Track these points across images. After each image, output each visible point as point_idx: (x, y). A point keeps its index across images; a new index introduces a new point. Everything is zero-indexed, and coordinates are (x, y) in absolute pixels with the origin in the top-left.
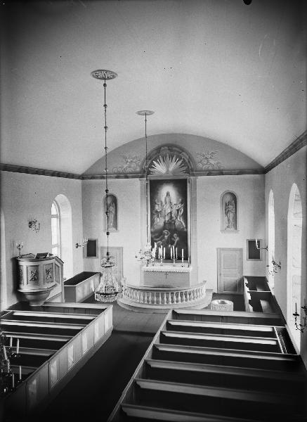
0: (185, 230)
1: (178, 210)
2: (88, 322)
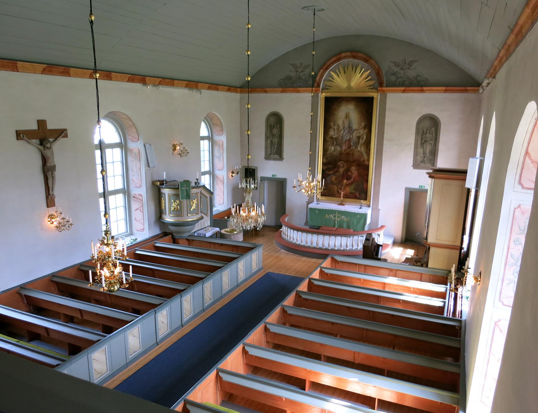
0: (367, 163)
1: (359, 138)
2: (230, 260)
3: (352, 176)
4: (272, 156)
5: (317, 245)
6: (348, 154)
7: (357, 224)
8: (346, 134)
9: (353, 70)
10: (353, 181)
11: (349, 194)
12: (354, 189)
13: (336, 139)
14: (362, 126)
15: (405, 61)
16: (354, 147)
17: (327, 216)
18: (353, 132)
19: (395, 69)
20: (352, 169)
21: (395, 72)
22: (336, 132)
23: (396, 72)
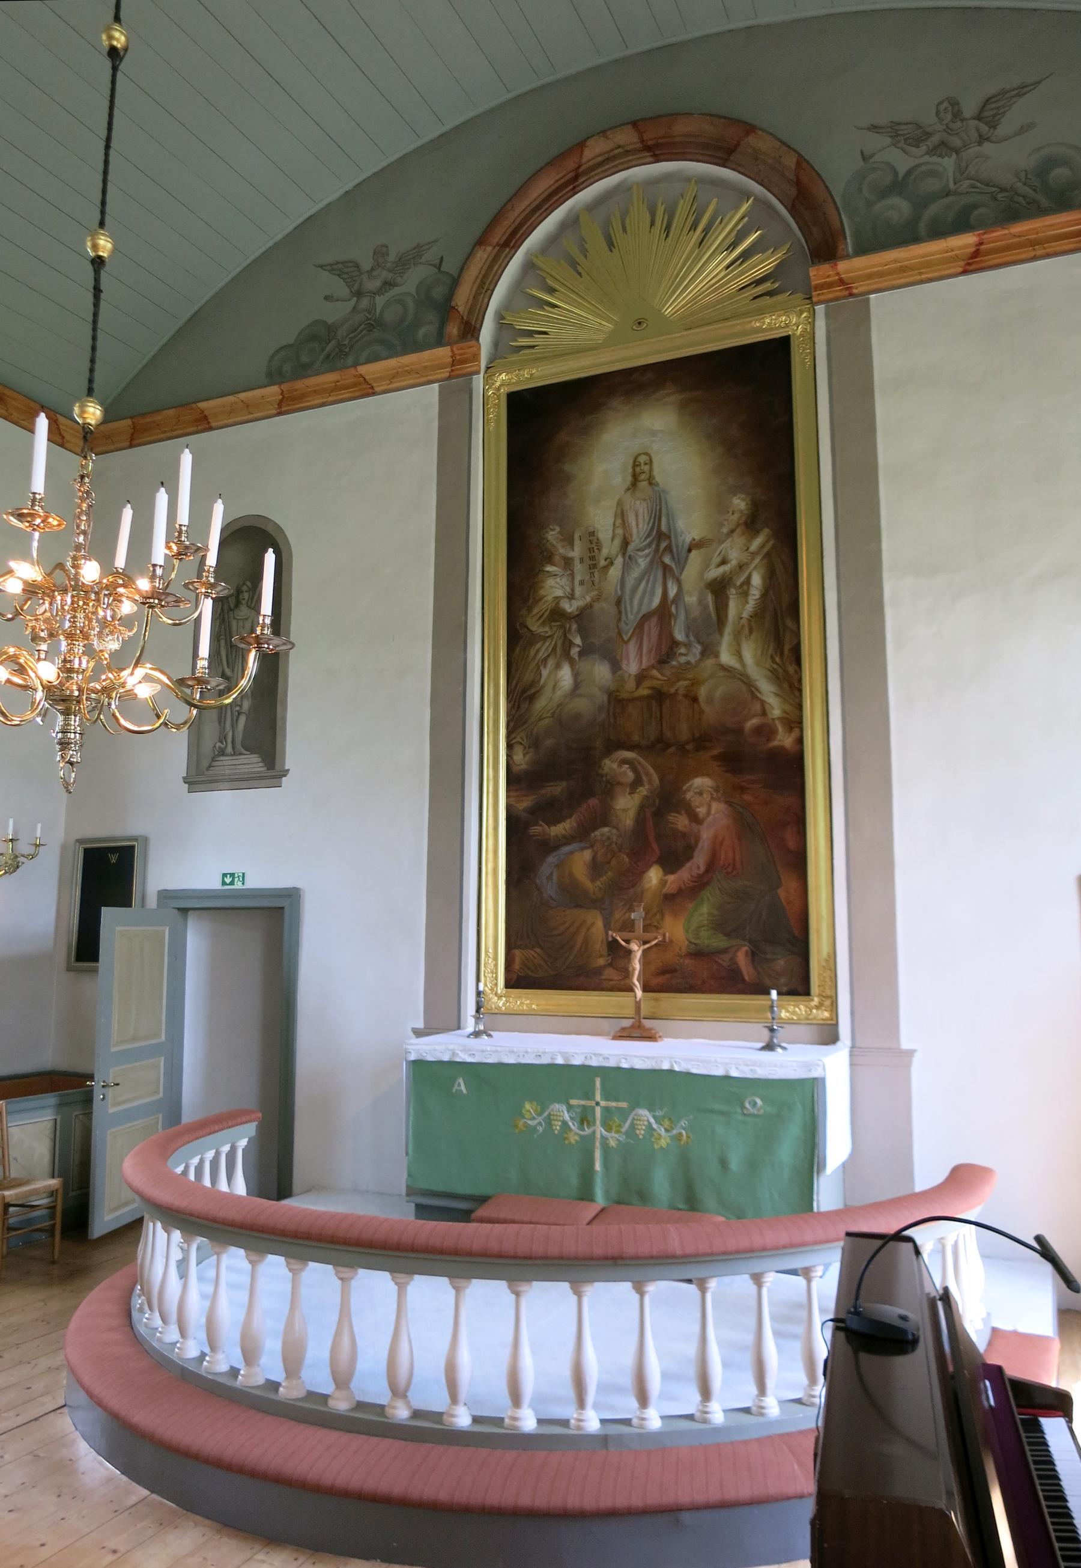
0: (784, 740)
1: (719, 588)
3: (697, 840)
4: (226, 765)
5: (342, 1380)
6: (659, 696)
7: (753, 1166)
8: (639, 581)
9: (652, 224)
10: (702, 869)
11: (687, 961)
12: (721, 925)
13: (582, 616)
14: (735, 517)
15: (954, 103)
16: (697, 649)
17: (530, 1112)
18: (682, 564)
19: (902, 161)
20: (689, 796)
21: (901, 176)
22: (578, 578)
23: (909, 173)
